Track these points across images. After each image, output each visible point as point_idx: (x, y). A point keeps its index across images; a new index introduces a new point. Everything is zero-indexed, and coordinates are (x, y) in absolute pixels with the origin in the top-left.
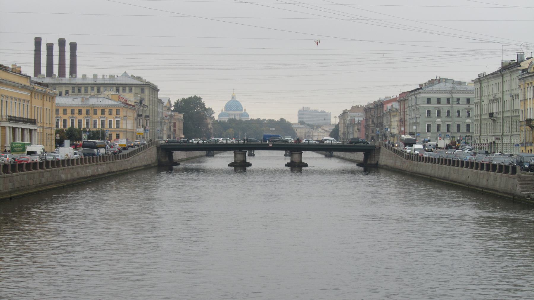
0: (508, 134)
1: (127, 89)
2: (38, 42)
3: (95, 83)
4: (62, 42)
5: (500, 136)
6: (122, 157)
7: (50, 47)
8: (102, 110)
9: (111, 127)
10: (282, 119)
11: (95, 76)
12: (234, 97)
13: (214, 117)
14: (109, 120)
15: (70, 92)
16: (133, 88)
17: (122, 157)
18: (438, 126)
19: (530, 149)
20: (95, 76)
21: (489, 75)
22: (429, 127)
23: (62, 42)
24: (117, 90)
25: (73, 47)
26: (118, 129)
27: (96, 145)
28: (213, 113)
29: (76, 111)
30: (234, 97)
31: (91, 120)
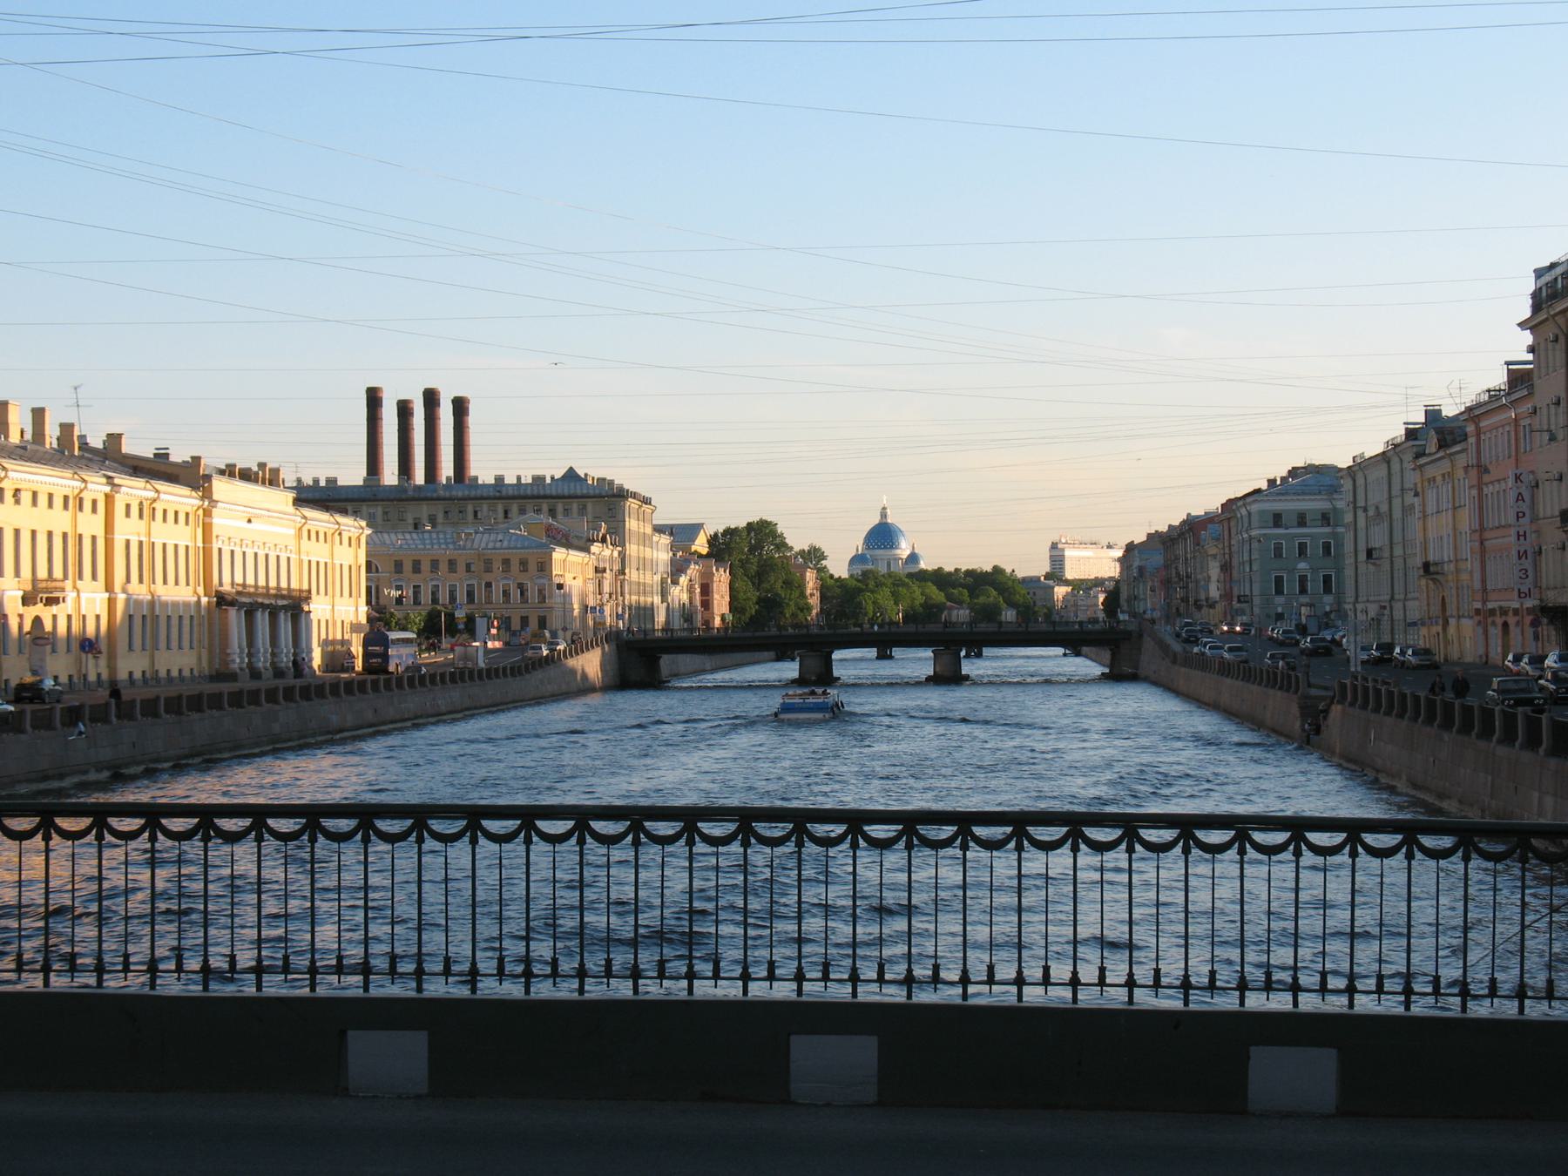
0: (1416, 595)
1: (575, 506)
2: (374, 399)
3: (498, 494)
4: (431, 398)
5: (1385, 601)
6: (508, 672)
7: (404, 409)
8: (432, 561)
9: (420, 604)
10: (995, 568)
11: (316, 481)
12: (884, 515)
13: (825, 567)
14: (414, 587)
15: (440, 518)
16: (590, 507)
17: (508, 672)
18: (1303, 580)
19: (415, 688)
20: (316, 481)
21: (1371, 458)
22: (1279, 580)
23: (431, 398)
24: (550, 510)
25: (460, 406)
26: (524, 605)
27: (675, 635)
28: (824, 558)
29: (408, 566)
30: (884, 515)
31: (444, 586)
